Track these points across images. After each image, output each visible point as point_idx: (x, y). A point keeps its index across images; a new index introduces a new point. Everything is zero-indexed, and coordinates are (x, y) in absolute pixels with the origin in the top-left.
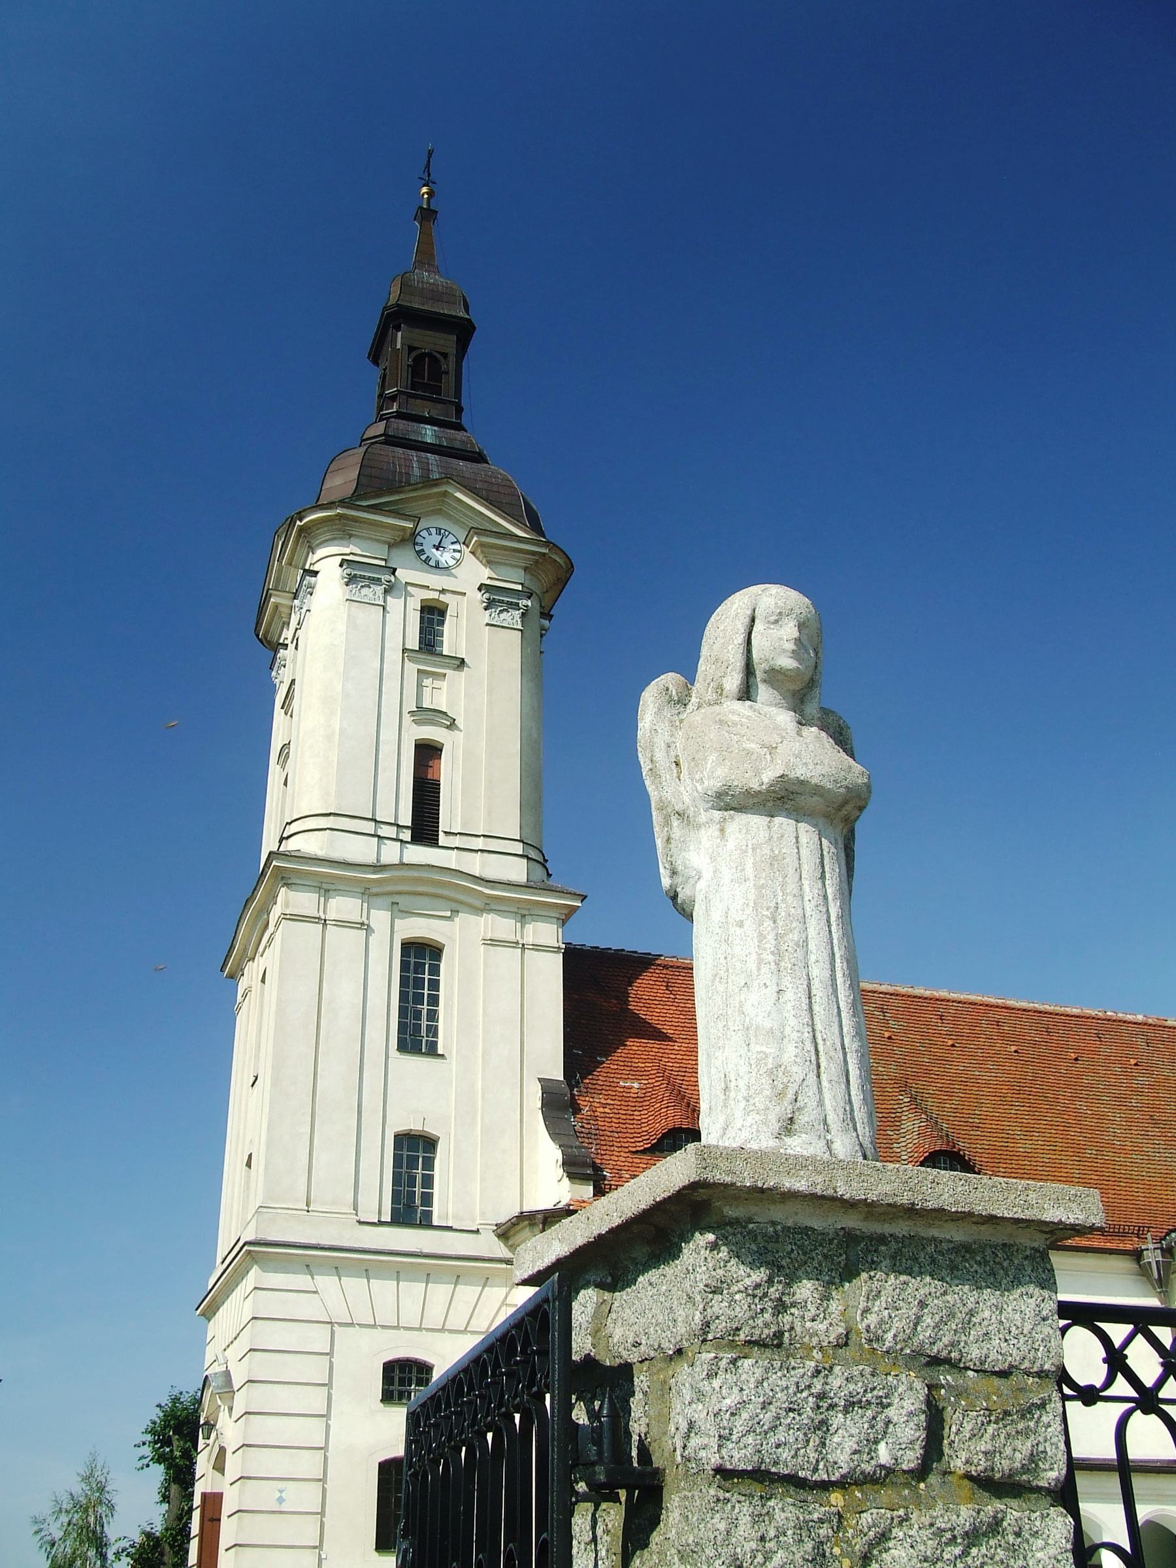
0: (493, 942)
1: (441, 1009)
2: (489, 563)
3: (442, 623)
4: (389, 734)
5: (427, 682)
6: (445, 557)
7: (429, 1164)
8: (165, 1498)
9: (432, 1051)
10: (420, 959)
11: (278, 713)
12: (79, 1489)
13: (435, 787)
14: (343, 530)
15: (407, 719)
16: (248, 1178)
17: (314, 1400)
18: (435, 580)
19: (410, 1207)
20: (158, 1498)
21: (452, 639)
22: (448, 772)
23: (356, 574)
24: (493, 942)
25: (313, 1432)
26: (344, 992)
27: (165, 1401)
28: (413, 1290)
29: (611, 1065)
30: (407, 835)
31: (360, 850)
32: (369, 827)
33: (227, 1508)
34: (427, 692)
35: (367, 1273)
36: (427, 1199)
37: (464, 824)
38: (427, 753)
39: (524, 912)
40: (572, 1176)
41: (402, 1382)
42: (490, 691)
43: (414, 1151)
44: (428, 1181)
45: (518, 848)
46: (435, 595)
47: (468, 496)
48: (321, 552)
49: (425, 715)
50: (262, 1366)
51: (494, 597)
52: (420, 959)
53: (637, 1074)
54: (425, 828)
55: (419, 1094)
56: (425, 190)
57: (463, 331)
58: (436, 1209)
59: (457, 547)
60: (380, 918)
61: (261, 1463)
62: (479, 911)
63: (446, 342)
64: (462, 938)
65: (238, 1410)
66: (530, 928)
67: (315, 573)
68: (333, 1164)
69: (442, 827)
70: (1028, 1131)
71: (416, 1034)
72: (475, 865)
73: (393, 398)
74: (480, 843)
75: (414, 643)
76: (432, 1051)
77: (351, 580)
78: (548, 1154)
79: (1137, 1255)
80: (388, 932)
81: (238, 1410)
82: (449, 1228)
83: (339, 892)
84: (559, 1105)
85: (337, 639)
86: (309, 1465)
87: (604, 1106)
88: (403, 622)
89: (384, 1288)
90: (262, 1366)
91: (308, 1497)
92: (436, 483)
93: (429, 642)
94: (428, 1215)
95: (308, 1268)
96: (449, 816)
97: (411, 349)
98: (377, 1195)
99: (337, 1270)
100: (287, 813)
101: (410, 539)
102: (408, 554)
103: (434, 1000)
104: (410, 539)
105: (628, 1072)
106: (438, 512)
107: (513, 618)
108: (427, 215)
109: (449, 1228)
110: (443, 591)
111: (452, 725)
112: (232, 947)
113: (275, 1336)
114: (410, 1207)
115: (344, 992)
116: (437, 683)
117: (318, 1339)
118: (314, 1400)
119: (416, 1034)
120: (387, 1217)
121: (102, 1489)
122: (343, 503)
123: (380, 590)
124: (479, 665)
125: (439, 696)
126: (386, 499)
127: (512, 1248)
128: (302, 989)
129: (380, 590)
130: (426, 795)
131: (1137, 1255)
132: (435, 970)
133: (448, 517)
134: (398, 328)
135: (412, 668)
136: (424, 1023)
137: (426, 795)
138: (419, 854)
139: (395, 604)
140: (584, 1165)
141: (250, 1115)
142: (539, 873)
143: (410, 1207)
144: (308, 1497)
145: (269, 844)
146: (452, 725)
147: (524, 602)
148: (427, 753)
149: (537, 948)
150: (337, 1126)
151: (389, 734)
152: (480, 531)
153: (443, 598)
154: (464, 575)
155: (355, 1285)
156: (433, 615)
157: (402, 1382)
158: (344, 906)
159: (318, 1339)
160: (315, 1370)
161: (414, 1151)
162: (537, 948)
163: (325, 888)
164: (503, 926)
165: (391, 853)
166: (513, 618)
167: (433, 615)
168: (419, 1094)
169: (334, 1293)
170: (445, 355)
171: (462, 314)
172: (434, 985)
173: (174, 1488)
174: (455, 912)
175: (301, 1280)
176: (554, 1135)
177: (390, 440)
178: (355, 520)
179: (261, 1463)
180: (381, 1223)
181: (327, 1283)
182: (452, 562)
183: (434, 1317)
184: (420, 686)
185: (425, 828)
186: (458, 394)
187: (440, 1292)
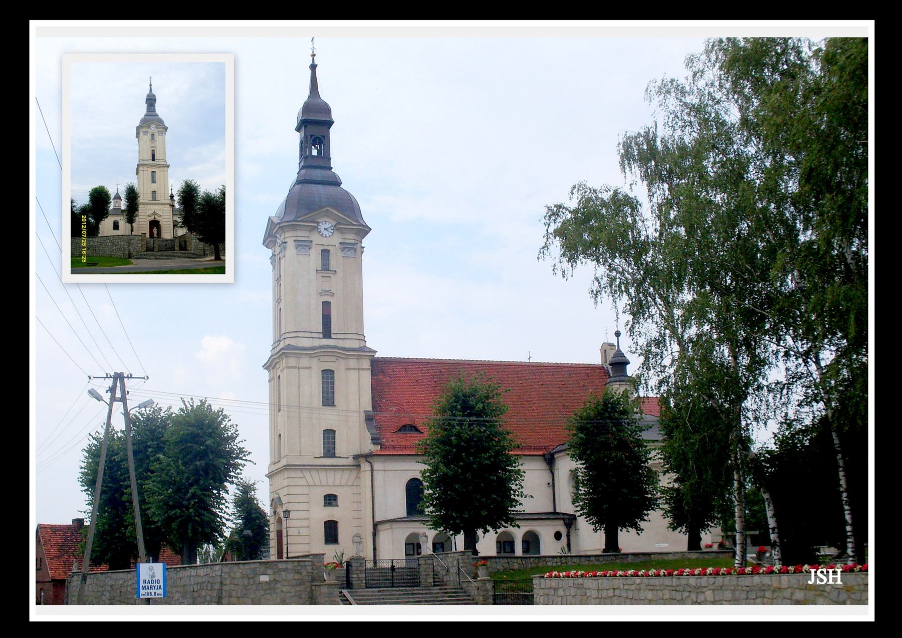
9: (333, 405)
10: (328, 376)
21: (333, 265)
30: (321, 336)
38: (326, 305)
47: (583, 600)
48: (287, 235)
52: (328, 376)
54: (327, 332)
55: (329, 418)
57: (330, 123)
71: (328, 400)
72: (341, 344)
74: (342, 336)
76: (333, 405)
80: (316, 367)
88: (314, 259)
90: (291, 498)
93: (326, 266)
96: (334, 329)
97: (311, 136)
98: (320, 450)
113: (293, 490)
119: (328, 400)
130: (153, 156)
137: (153, 156)
148: (326, 305)
155: (315, 474)
156: (325, 253)
158: (305, 362)
163: (298, 356)
165: (317, 343)
181: (307, 474)
185: (327, 332)
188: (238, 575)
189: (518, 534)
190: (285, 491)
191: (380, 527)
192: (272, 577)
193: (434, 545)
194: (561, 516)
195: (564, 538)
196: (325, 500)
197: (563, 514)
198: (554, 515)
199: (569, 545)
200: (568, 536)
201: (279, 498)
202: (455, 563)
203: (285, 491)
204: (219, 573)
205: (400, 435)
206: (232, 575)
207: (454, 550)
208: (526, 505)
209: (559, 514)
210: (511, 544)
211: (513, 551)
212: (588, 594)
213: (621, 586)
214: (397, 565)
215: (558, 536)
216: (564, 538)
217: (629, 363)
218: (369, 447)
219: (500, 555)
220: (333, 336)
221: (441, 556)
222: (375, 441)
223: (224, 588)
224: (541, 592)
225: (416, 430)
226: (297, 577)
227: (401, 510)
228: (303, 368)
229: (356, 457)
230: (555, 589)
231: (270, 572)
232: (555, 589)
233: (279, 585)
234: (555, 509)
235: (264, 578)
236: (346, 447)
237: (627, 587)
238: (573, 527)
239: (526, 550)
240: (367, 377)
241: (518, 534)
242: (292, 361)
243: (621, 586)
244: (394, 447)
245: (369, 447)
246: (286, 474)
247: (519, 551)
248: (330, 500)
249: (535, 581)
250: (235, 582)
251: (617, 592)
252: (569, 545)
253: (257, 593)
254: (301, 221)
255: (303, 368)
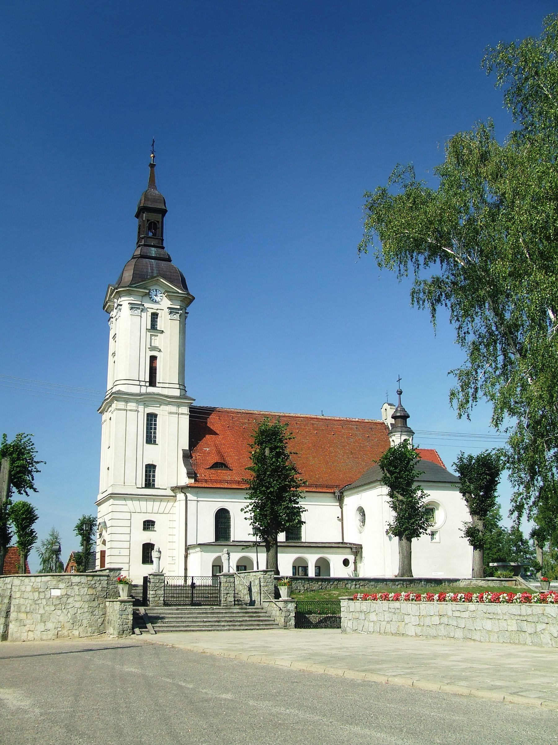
0: (171, 413)
1: (157, 431)
2: (170, 300)
3: (157, 318)
4: (142, 355)
5: (153, 337)
6: (158, 299)
7: (154, 472)
8: (82, 545)
9: (155, 443)
10: (151, 418)
11: (111, 340)
12: (49, 538)
13: (155, 369)
14: (129, 293)
15: (148, 350)
16: (108, 475)
17: (127, 530)
18: (155, 306)
19: (149, 483)
20: (80, 545)
21: (160, 325)
22: (159, 364)
23: (133, 307)
24: (171, 413)
25: (127, 538)
26: (132, 428)
27: (81, 518)
28: (150, 504)
29: (201, 443)
30: (148, 384)
31: (135, 390)
32: (138, 383)
33: (107, 554)
34: (153, 340)
35: (139, 500)
36: (154, 481)
37: (163, 380)
38: (153, 359)
39: (179, 405)
40: (189, 477)
41: (148, 525)
42: (170, 340)
43: (150, 469)
44: (154, 476)
45: (178, 386)
46: (155, 311)
48: (123, 299)
49: (153, 348)
50: (115, 523)
51: (172, 311)
52: (151, 418)
53: (208, 446)
54: (152, 382)
55: (151, 454)
56: (152, 155)
57: (164, 212)
58: (156, 483)
59: (161, 295)
60: (141, 408)
61: (115, 544)
62: (167, 405)
63: (158, 217)
64: (163, 413)
65: (108, 532)
66: (180, 409)
67: (121, 305)
68: (130, 473)
69: (157, 381)
70: (314, 458)
71: (151, 439)
72: (166, 392)
73: (143, 238)
74: (167, 385)
75: (149, 327)
76: (155, 443)
77: (131, 308)
78: (183, 471)
79: (334, 493)
80: (144, 411)
81: (108, 532)
82: (159, 488)
83: (131, 402)
84: (187, 456)
85: (126, 324)
86: (126, 545)
87: (199, 456)
88: (146, 318)
89: (143, 503)
90: (115, 523)
91: (126, 552)
92: (155, 277)
94: (154, 485)
95: (125, 499)
96: (159, 377)
97: (148, 220)
98: (141, 481)
99: (132, 499)
100: (115, 376)
101: (148, 294)
102: (147, 298)
103: (155, 429)
104: (148, 294)
105: (207, 445)
106: (156, 284)
107: (177, 316)
108: (152, 166)
109: (159, 488)
110: (157, 309)
111: (160, 351)
112: (101, 407)
114: (149, 483)
115: (132, 428)
116: (156, 338)
117: (128, 516)
118: (127, 530)
119: (151, 439)
120: (144, 486)
121: (57, 538)
122: (128, 286)
123: (139, 311)
124: (167, 332)
125: (156, 343)
126: (140, 283)
127: (175, 493)
128: (119, 428)
129: (139, 311)
131: (334, 493)
132: (155, 421)
133: (159, 285)
134: (144, 213)
135: (149, 334)
136: (153, 435)
138: (151, 390)
139: (144, 314)
140: (192, 474)
141: (107, 457)
142: (183, 392)
143: (150, 484)
144: (126, 552)
145: (109, 386)
146: (160, 351)
147: (180, 312)
148: (153, 359)
149: (182, 414)
150: (131, 464)
151: (142, 355)
152: (166, 291)
153: (158, 311)
154: (163, 304)
155: (136, 503)
156: (155, 316)
157: (148, 525)
158: (132, 405)
159: (128, 516)
160: (127, 523)
161: (150, 469)
162: (182, 414)
163: (127, 401)
164: (174, 409)
165: (143, 390)
166: (177, 316)
167: (155, 316)
168: (151, 454)
169: (131, 505)
170: (158, 222)
171: (164, 207)
172: (155, 425)
173: (85, 542)
174: (161, 405)
175: (123, 502)
176: (186, 465)
177: (143, 256)
178: (132, 290)
179: (115, 544)
180: (142, 488)
181: (129, 503)
182: (160, 300)
183: (155, 510)
184: (151, 339)
185: (152, 382)
186: (162, 236)
187: (157, 504)
188: (29, 588)
189: (312, 559)
190: (109, 516)
191: (190, 551)
192: (64, 592)
193: (238, 567)
194: (348, 545)
195: (351, 564)
196: (144, 525)
197: (350, 544)
198: (341, 546)
199: (356, 569)
200: (355, 563)
201: (105, 522)
202: (257, 582)
203: (109, 516)
204: (9, 586)
205: (213, 471)
206: (23, 588)
207: (255, 569)
208: (308, 534)
209: (346, 543)
210: (305, 568)
211: (306, 574)
212: (406, 621)
213: (450, 613)
214: (197, 582)
215: (346, 563)
216: (351, 564)
217: (408, 417)
218: (184, 480)
219: (294, 577)
220: (157, 385)
221: (242, 575)
222: (191, 474)
223: (13, 602)
224: (350, 616)
225: (226, 466)
226: (91, 591)
227: (211, 537)
228: (131, 410)
229: (174, 489)
230: (367, 613)
231: (62, 585)
232: (367, 613)
233: (70, 600)
234: (343, 539)
235: (56, 593)
236: (162, 479)
237: (457, 614)
238: (359, 555)
239: (318, 573)
240: (185, 422)
241: (312, 559)
242: (121, 405)
243: (450, 613)
244: (206, 481)
245: (184, 480)
246: (111, 501)
247: (312, 573)
248: (148, 525)
249: (344, 603)
250: (26, 595)
251: (445, 620)
252: (356, 569)
253: (47, 608)
254: (135, 287)
255: (131, 410)
